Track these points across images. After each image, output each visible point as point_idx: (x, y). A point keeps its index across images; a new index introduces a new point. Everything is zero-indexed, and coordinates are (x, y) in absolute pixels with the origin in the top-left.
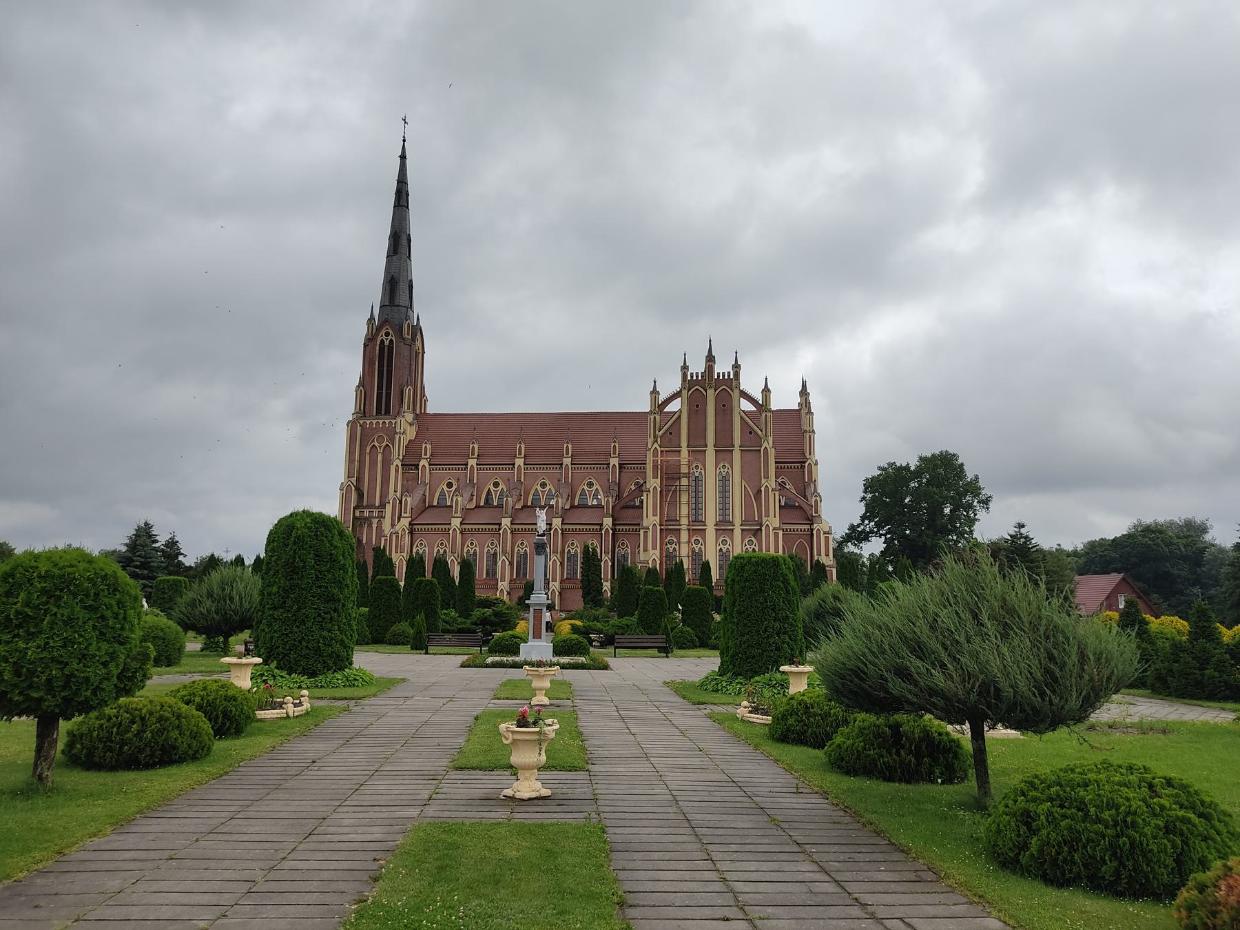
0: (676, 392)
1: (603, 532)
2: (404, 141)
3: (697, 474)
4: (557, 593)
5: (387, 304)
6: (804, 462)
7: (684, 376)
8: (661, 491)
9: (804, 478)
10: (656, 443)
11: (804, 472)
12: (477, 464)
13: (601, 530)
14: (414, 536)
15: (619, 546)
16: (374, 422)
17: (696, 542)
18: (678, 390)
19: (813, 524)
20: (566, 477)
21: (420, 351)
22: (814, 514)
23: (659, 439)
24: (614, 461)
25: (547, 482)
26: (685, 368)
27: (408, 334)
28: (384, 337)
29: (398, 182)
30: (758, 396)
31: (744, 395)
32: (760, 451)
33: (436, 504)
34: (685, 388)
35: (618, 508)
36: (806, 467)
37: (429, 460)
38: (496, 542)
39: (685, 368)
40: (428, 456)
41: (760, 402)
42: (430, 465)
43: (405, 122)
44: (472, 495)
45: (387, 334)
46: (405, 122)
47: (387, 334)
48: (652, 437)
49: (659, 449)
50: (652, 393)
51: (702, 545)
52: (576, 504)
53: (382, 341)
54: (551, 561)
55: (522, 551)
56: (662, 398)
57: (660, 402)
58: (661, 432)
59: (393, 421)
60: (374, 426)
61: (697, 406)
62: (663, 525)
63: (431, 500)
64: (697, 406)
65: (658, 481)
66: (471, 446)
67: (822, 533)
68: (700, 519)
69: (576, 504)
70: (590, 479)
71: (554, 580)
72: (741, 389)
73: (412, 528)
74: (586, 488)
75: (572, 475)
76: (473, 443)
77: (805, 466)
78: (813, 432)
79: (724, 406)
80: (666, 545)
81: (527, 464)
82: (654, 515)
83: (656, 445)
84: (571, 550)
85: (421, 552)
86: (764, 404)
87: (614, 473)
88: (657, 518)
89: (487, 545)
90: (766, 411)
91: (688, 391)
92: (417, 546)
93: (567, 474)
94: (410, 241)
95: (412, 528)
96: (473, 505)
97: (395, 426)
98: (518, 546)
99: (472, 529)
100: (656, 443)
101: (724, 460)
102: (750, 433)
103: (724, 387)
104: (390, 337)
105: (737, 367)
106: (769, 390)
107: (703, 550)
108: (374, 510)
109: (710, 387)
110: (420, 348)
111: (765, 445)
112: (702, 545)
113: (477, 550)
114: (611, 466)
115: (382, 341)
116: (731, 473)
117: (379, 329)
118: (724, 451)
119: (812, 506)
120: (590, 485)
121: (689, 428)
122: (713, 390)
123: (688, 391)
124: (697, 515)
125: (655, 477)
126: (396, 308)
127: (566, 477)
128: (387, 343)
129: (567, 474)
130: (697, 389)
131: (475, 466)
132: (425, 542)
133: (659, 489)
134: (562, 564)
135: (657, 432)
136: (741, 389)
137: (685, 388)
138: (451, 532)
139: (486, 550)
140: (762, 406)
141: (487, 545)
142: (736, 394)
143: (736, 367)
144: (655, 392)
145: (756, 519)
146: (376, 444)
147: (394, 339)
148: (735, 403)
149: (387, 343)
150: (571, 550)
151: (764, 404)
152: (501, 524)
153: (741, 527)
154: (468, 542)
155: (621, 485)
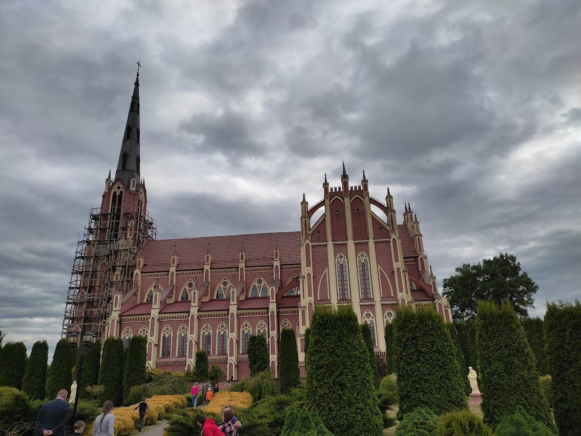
0: (320, 202)
1: (269, 314)
2: (138, 75)
3: (341, 262)
4: (234, 366)
5: (120, 170)
6: (417, 257)
7: (326, 189)
8: (313, 277)
9: (418, 268)
10: (307, 240)
11: (417, 265)
12: (176, 271)
13: (268, 313)
14: (122, 325)
15: (243, 327)
17: (368, 316)
18: (322, 200)
19: (434, 300)
20: (242, 277)
21: (144, 200)
22: (433, 293)
23: (310, 237)
24: (277, 263)
25: (228, 281)
26: (326, 185)
27: (133, 187)
28: (117, 190)
29: (133, 98)
30: (384, 202)
31: (373, 201)
32: (390, 242)
33: (146, 302)
34: (327, 198)
35: (280, 296)
36: (419, 260)
37: (141, 269)
38: (225, 325)
39: (326, 185)
40: (141, 267)
41: (386, 206)
42: (142, 273)
43: (139, 65)
44: (171, 293)
45: (119, 188)
46: (139, 65)
47: (119, 188)
48: (304, 235)
49: (310, 244)
50: (302, 203)
51: (372, 318)
52: (250, 296)
53: (115, 193)
54: (229, 339)
55: (206, 334)
56: (310, 206)
57: (309, 210)
58: (311, 231)
61: (338, 211)
62: (317, 304)
63: (142, 299)
64: (338, 211)
65: (311, 268)
67: (443, 306)
68: (347, 298)
69: (250, 296)
70: (259, 277)
71: (231, 355)
72: (370, 197)
73: (120, 319)
74: (257, 284)
75: (246, 275)
76: (174, 255)
77: (418, 260)
78: (421, 235)
79: (358, 210)
80: (386, 317)
81: (212, 269)
82: (310, 295)
83: (308, 241)
84: (245, 330)
85: (167, 336)
86: (389, 207)
87: (277, 272)
88: (312, 298)
89: (218, 328)
90: (391, 212)
91: (330, 200)
92: (124, 333)
93: (242, 274)
94: (139, 133)
95: (120, 319)
96: (172, 300)
98: (204, 329)
99: (178, 317)
100: (307, 240)
101: (362, 250)
102: (381, 229)
103: (357, 196)
104: (120, 190)
105: (365, 182)
106: (391, 196)
107: (374, 322)
109: (347, 197)
110: (144, 198)
111: (393, 236)
112: (372, 318)
113: (211, 332)
114: (274, 267)
115: (115, 193)
116: (368, 261)
117: (114, 184)
118: (361, 247)
119: (431, 286)
120: (260, 281)
121: (332, 228)
122: (349, 198)
123: (330, 200)
124: (343, 294)
125: (308, 265)
126: (126, 172)
127: (242, 277)
128: (118, 194)
129: (242, 274)
130: (336, 198)
131: (175, 272)
132: (170, 328)
133: (312, 275)
134: (238, 342)
135: (308, 232)
136: (370, 197)
137: (327, 198)
138: (150, 320)
139: (178, 335)
140: (387, 208)
141: (218, 328)
142: (367, 201)
143: (365, 181)
144: (304, 203)
145: (392, 295)
147: (123, 191)
148: (366, 206)
149: (118, 194)
150: (245, 330)
151: (389, 207)
152: (189, 312)
153: (381, 302)
154: (165, 328)
155: (283, 281)
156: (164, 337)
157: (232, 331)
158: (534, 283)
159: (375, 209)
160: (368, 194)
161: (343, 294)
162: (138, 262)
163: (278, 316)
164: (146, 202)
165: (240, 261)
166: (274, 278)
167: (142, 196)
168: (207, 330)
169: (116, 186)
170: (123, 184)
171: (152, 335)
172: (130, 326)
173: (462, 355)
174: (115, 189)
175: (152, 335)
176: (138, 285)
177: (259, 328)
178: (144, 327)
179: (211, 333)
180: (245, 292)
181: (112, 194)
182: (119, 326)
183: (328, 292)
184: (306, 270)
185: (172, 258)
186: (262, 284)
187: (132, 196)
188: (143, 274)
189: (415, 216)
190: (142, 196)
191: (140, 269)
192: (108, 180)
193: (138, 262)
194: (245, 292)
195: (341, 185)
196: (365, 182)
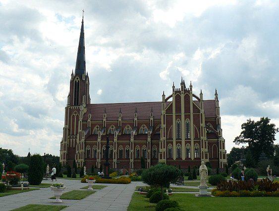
7: (173, 90)
26: (174, 87)
30: (199, 97)
31: (194, 96)
39: (174, 87)
47: (77, 79)
56: (166, 97)
71: (132, 159)
82: (164, 148)
88: (165, 149)
117: (75, 77)
124: (179, 136)
125: (164, 124)
134: (134, 153)
142: (191, 95)
156: (120, 150)
157: (149, 149)
159: (194, 99)
160: (191, 93)
161: (179, 136)
163: (151, 144)
167: (87, 81)
168: (121, 148)
171: (99, 149)
173: (270, 171)
174: (76, 79)
175: (99, 149)
184: (163, 126)
190: (87, 81)
192: (72, 74)
195: (180, 88)
196: (191, 86)
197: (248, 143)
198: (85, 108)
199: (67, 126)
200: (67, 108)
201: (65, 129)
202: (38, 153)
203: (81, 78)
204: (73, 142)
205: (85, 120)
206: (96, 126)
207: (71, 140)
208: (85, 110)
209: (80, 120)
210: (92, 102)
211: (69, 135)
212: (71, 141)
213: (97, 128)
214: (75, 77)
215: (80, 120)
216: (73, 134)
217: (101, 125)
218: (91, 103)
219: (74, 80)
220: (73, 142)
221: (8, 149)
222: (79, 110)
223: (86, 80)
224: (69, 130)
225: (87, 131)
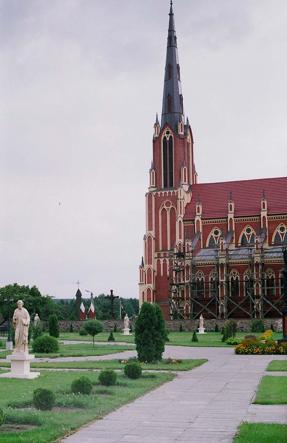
12: (234, 217)
16: (163, 192)
25: (284, 226)
27: (182, 131)
28: (166, 135)
42: (202, 219)
45: (168, 133)
47: (168, 133)
53: (165, 138)
59: (176, 191)
60: (167, 195)
66: (229, 205)
97: (177, 195)
104: (170, 135)
108: (167, 252)
113: (238, 277)
115: (165, 138)
117: (162, 131)
128: (168, 139)
131: (266, 217)
146: (165, 207)
149: (168, 139)
158: (28, 287)
162: (197, 209)
164: (193, 142)
165: (262, 209)
166: (196, 232)
167: (189, 137)
169: (165, 132)
170: (172, 129)
171: (222, 278)
172: (201, 270)
174: (164, 135)
176: (200, 232)
177: (268, 275)
178: (200, 272)
179: (239, 278)
180: (234, 240)
181: (162, 139)
182: (192, 269)
183: (147, 256)
185: (229, 205)
186: (251, 233)
187: (181, 140)
188: (202, 221)
189: (187, 119)
191: (199, 215)
192: (157, 124)
193: (197, 209)
194: (234, 240)
197: (39, 373)
198: (187, 192)
199: (153, 233)
200: (149, 196)
201: (148, 239)
202: (100, 294)
203: (176, 131)
204: (165, 265)
205: (189, 217)
206: (214, 230)
207: (162, 260)
208: (188, 198)
209: (180, 217)
210: (200, 180)
211: (157, 249)
212: (162, 263)
213: (216, 233)
214: (162, 131)
215: (180, 217)
216: (165, 249)
217: (224, 227)
218: (198, 182)
219: (160, 135)
220: (165, 265)
221: (108, 293)
222: (175, 199)
223: (186, 134)
224: (156, 240)
225: (196, 240)
